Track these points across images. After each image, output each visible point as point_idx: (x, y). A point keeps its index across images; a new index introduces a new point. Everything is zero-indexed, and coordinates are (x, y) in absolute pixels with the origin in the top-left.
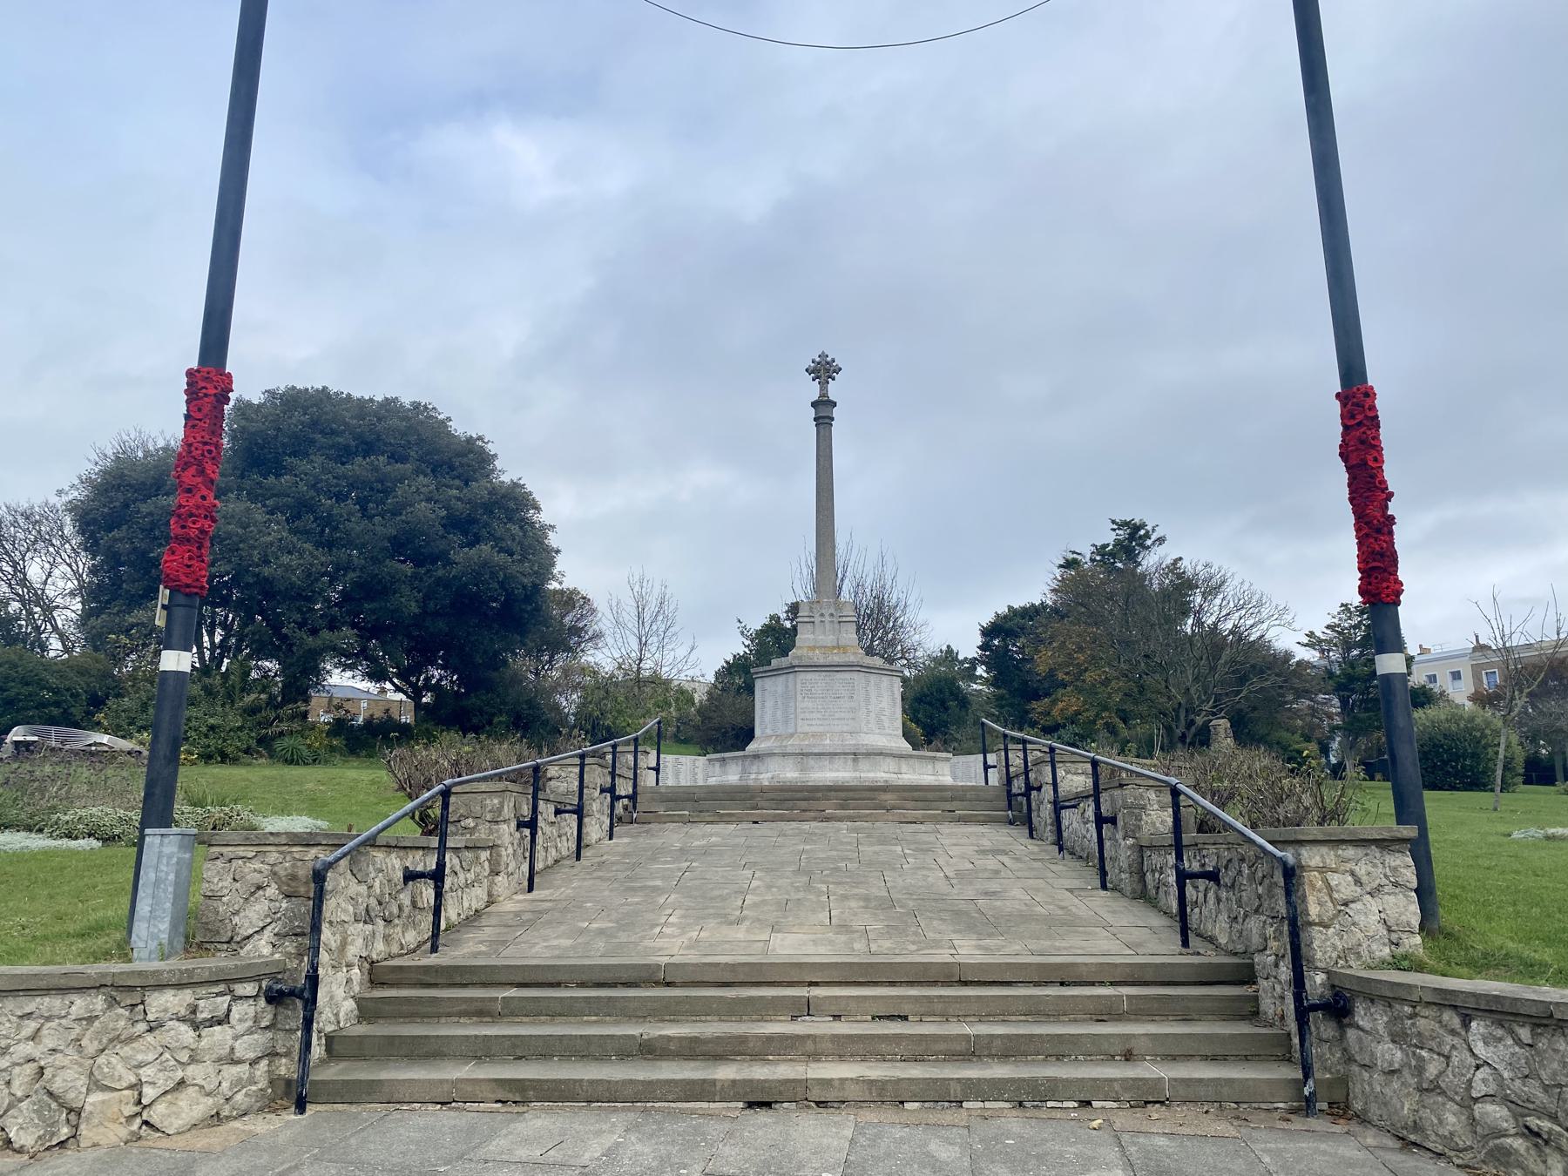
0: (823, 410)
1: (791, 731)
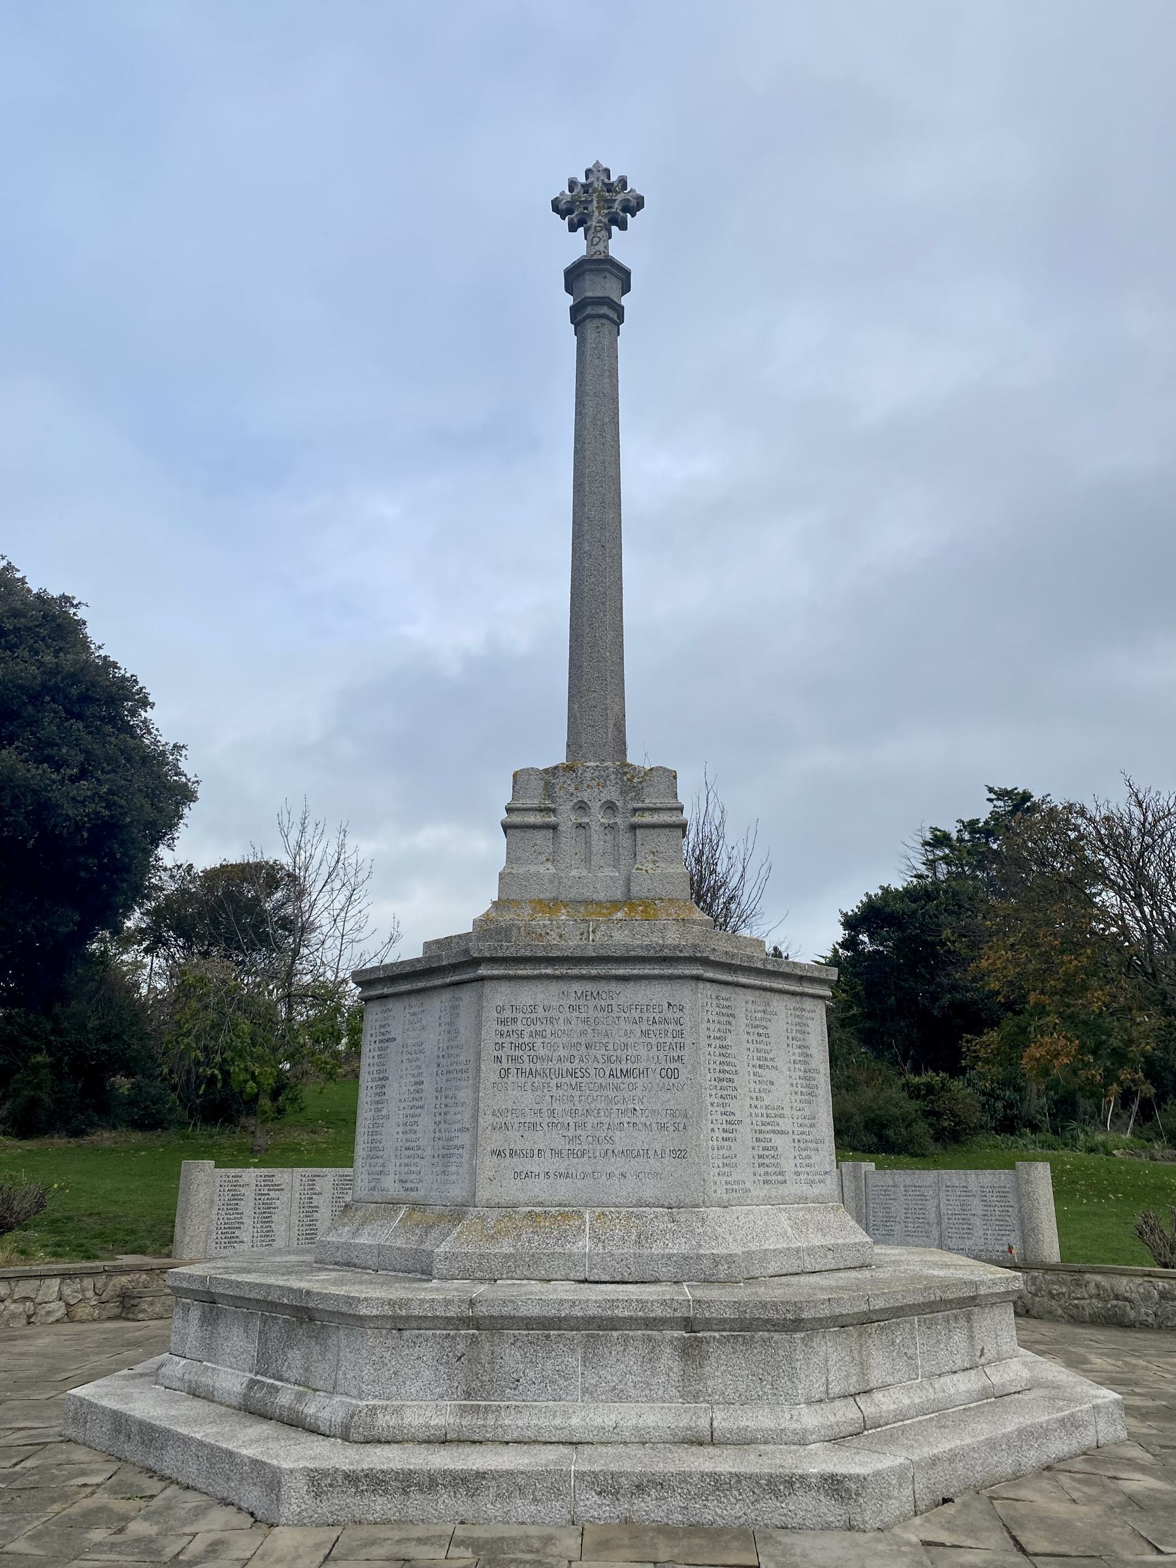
0: (596, 297)
1: (457, 1192)
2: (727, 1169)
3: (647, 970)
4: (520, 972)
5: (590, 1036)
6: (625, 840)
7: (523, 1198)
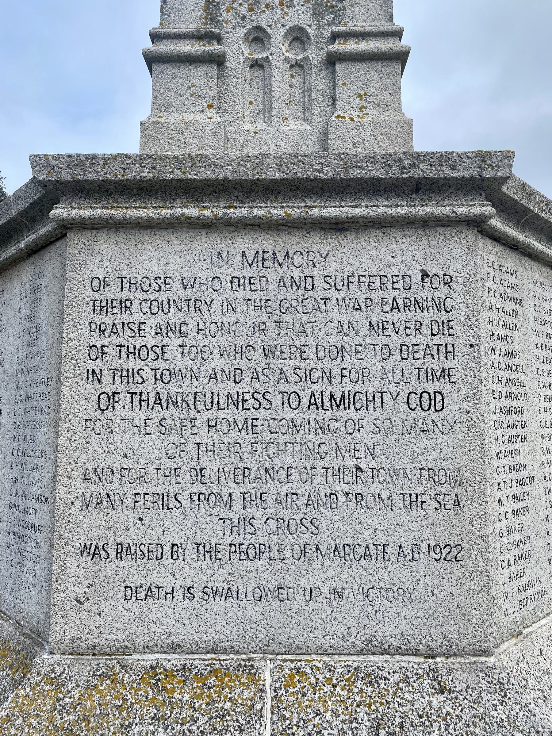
3: (383, 208)
4: (133, 213)
5: (271, 333)
6: (319, 80)
7: (140, 636)
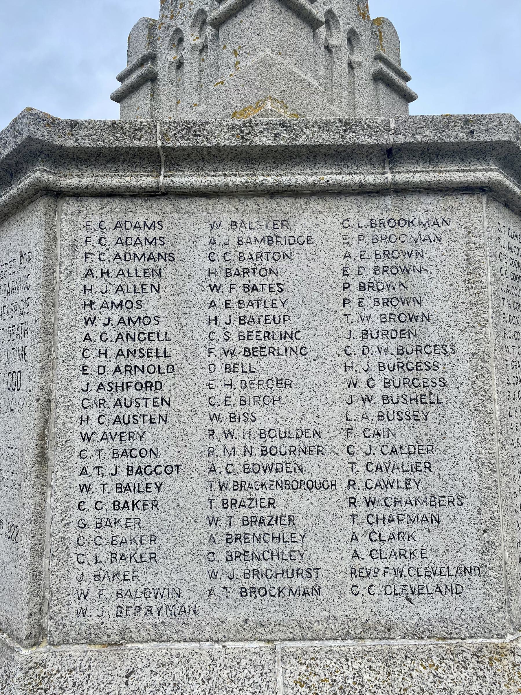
2: (120, 567)
